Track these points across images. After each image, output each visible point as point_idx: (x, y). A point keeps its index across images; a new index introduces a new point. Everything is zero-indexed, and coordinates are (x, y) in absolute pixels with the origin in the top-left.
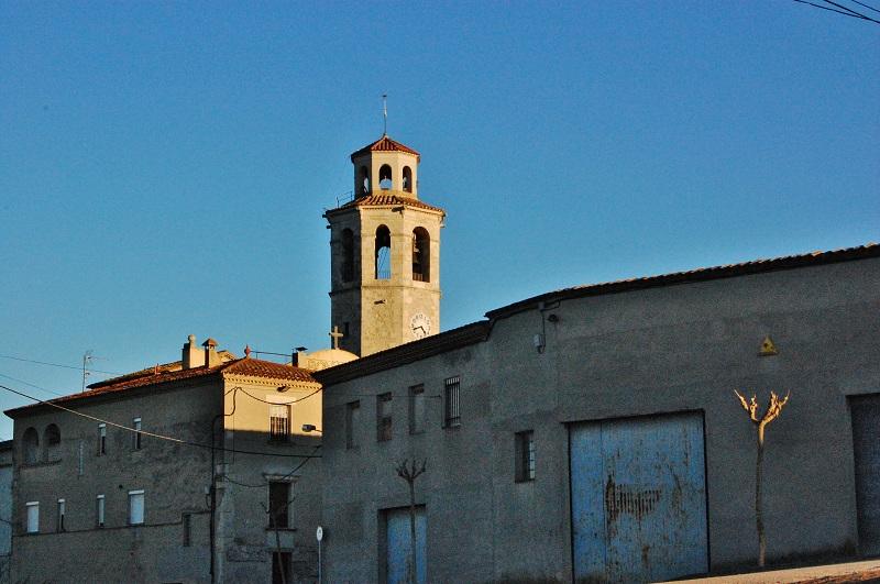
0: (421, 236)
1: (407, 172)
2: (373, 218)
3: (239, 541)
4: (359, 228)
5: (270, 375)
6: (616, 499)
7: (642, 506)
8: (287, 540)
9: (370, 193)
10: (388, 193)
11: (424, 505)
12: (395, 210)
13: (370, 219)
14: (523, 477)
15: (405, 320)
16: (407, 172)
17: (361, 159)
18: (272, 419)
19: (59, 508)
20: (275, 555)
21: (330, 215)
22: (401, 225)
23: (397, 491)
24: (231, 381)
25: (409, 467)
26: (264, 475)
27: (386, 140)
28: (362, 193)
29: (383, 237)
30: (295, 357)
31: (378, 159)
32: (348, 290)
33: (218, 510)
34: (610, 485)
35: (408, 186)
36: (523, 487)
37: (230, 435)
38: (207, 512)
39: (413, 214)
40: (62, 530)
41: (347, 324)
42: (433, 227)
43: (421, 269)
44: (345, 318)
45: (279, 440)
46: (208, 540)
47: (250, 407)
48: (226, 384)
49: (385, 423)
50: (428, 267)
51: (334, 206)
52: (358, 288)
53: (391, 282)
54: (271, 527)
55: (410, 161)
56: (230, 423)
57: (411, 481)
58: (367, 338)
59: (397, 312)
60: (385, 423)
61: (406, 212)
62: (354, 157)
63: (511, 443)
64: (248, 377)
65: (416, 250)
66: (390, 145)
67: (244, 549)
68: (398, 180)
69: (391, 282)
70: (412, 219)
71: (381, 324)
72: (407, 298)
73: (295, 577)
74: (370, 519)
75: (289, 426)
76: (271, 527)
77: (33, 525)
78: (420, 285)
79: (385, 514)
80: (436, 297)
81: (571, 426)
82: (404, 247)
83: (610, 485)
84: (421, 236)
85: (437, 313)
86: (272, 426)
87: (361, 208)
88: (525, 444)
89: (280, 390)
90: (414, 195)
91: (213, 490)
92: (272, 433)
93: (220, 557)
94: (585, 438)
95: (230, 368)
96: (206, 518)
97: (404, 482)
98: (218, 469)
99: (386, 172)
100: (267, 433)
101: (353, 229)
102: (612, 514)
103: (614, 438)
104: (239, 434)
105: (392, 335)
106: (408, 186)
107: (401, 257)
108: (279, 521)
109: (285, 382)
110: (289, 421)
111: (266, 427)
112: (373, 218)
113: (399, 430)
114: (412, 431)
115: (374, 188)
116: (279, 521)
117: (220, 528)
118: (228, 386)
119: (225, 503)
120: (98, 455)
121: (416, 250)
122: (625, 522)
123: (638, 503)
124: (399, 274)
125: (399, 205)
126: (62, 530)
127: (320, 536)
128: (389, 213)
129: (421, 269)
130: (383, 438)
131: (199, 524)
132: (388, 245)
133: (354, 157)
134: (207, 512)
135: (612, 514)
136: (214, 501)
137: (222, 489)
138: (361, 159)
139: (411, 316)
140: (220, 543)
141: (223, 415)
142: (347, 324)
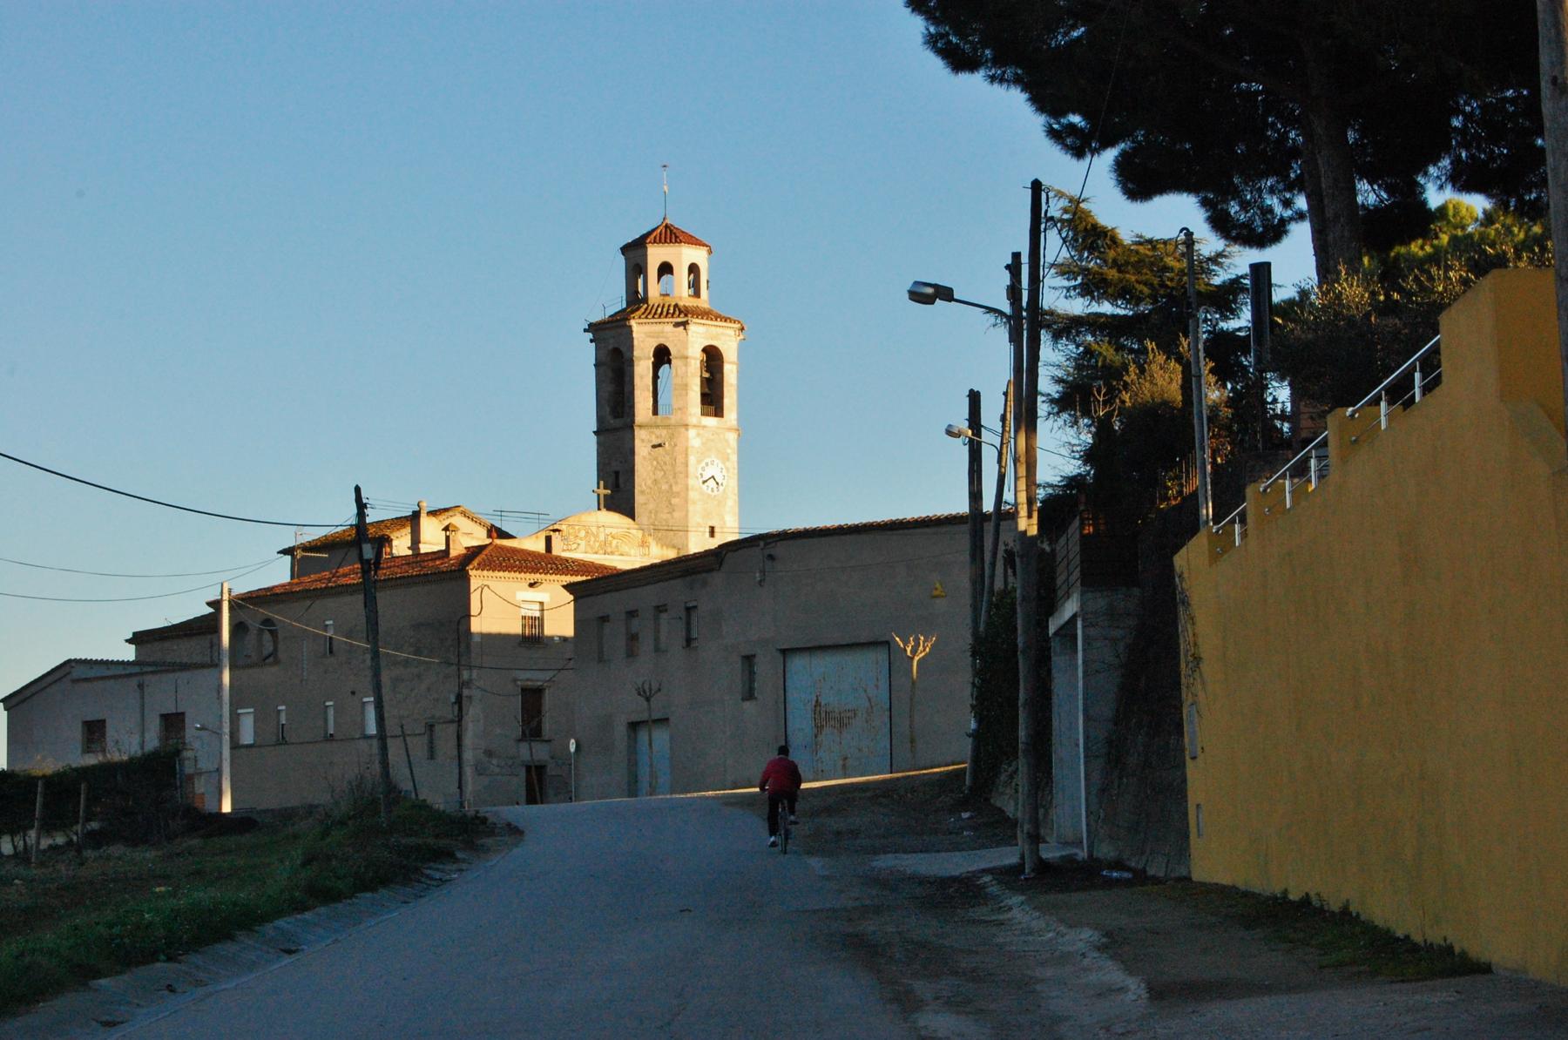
0: (713, 357)
1: (693, 269)
2: (649, 335)
3: (489, 753)
4: (632, 347)
5: (521, 569)
6: (823, 717)
7: (842, 723)
8: (541, 752)
9: (645, 300)
10: (668, 301)
11: (667, 719)
12: (677, 325)
13: (645, 336)
14: (749, 695)
15: (691, 469)
16: (693, 269)
17: (634, 252)
18: (524, 618)
19: (326, 713)
20: (528, 769)
21: (593, 328)
22: (685, 344)
23: (635, 708)
24: (478, 579)
25: (646, 687)
26: (515, 680)
27: (667, 226)
28: (636, 301)
29: (662, 356)
30: (548, 540)
31: (656, 255)
32: (616, 429)
33: (466, 718)
34: (818, 704)
35: (695, 286)
36: (747, 704)
37: (477, 639)
38: (452, 721)
39: (701, 329)
40: (282, 741)
41: (617, 473)
42: (728, 342)
43: (712, 400)
44: (615, 466)
45: (532, 640)
46: (455, 753)
47: (501, 606)
48: (473, 581)
49: (633, 638)
50: (722, 397)
51: (597, 317)
52: (630, 426)
53: (673, 420)
54: (524, 738)
55: (697, 255)
56: (478, 625)
57: (648, 700)
58: (642, 492)
59: (680, 459)
60: (633, 638)
61: (691, 327)
62: (625, 249)
63: (739, 665)
64: (497, 574)
65: (707, 375)
66: (670, 235)
67: (495, 761)
68: (681, 277)
69: (673, 420)
70: (698, 336)
71: (660, 474)
72: (693, 439)
73: (551, 792)
74: (621, 730)
75: (542, 626)
76: (524, 738)
77: (247, 737)
78: (712, 421)
79: (634, 726)
80: (732, 437)
81: (784, 652)
82: (688, 374)
83: (818, 704)
84: (713, 357)
85: (734, 458)
86: (524, 626)
87: (633, 323)
88: (751, 666)
89: (531, 585)
90: (704, 301)
91: (459, 698)
92: (523, 636)
93: (468, 771)
94: (797, 663)
95: (475, 563)
96: (453, 728)
97: (641, 700)
98: (465, 675)
99: (666, 269)
100: (515, 636)
101: (623, 349)
102: (819, 728)
103: (823, 664)
104: (489, 638)
105: (675, 489)
106: (695, 286)
107: (685, 387)
108: (532, 728)
109: (537, 577)
110: (541, 620)
111: (515, 628)
112: (649, 335)
113: (646, 645)
114: (657, 649)
115: (651, 294)
116: (532, 728)
117: (468, 740)
118: (475, 583)
119: (473, 712)
120: (324, 656)
121: (707, 375)
122: (828, 735)
123: (840, 720)
124: (683, 409)
125: (682, 315)
126: (282, 741)
127: (572, 748)
128: (669, 328)
129: (712, 400)
130: (631, 654)
131: (445, 735)
132: (669, 362)
133: (625, 249)
134: (452, 721)
135: (819, 728)
136: (460, 709)
137: (470, 697)
138: (634, 252)
139: (699, 462)
140: (468, 755)
141: (469, 616)
142: (617, 473)
